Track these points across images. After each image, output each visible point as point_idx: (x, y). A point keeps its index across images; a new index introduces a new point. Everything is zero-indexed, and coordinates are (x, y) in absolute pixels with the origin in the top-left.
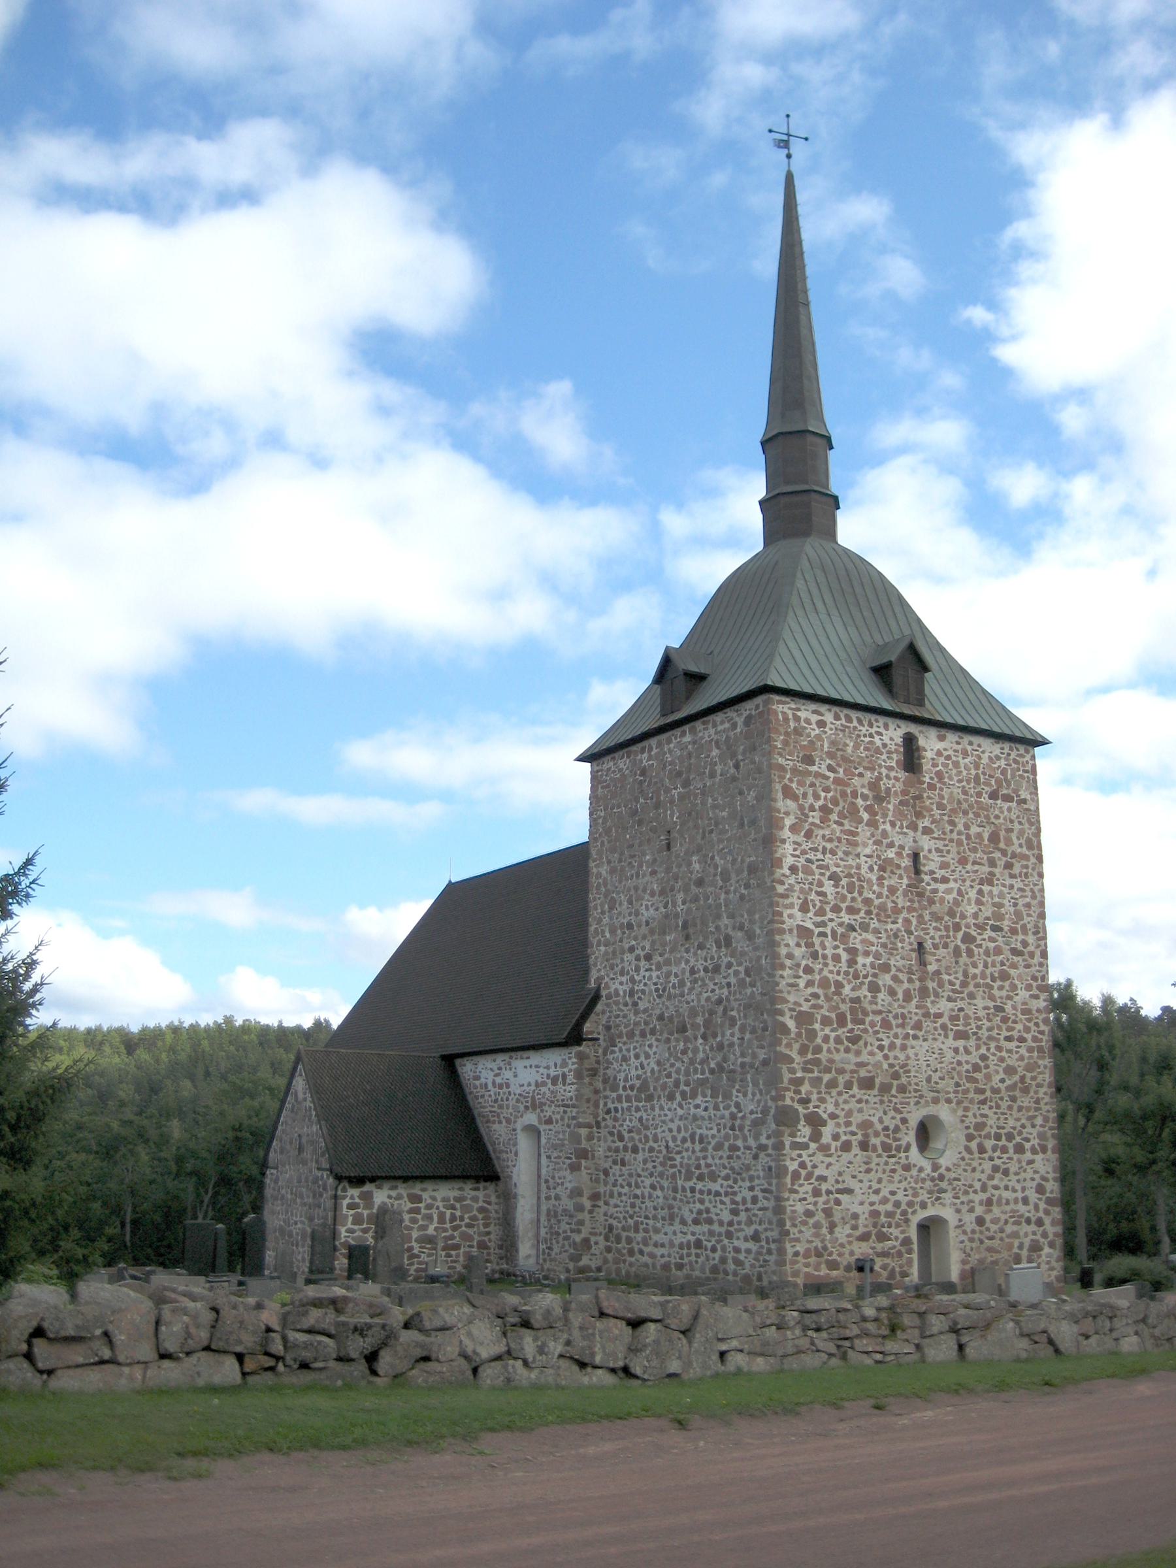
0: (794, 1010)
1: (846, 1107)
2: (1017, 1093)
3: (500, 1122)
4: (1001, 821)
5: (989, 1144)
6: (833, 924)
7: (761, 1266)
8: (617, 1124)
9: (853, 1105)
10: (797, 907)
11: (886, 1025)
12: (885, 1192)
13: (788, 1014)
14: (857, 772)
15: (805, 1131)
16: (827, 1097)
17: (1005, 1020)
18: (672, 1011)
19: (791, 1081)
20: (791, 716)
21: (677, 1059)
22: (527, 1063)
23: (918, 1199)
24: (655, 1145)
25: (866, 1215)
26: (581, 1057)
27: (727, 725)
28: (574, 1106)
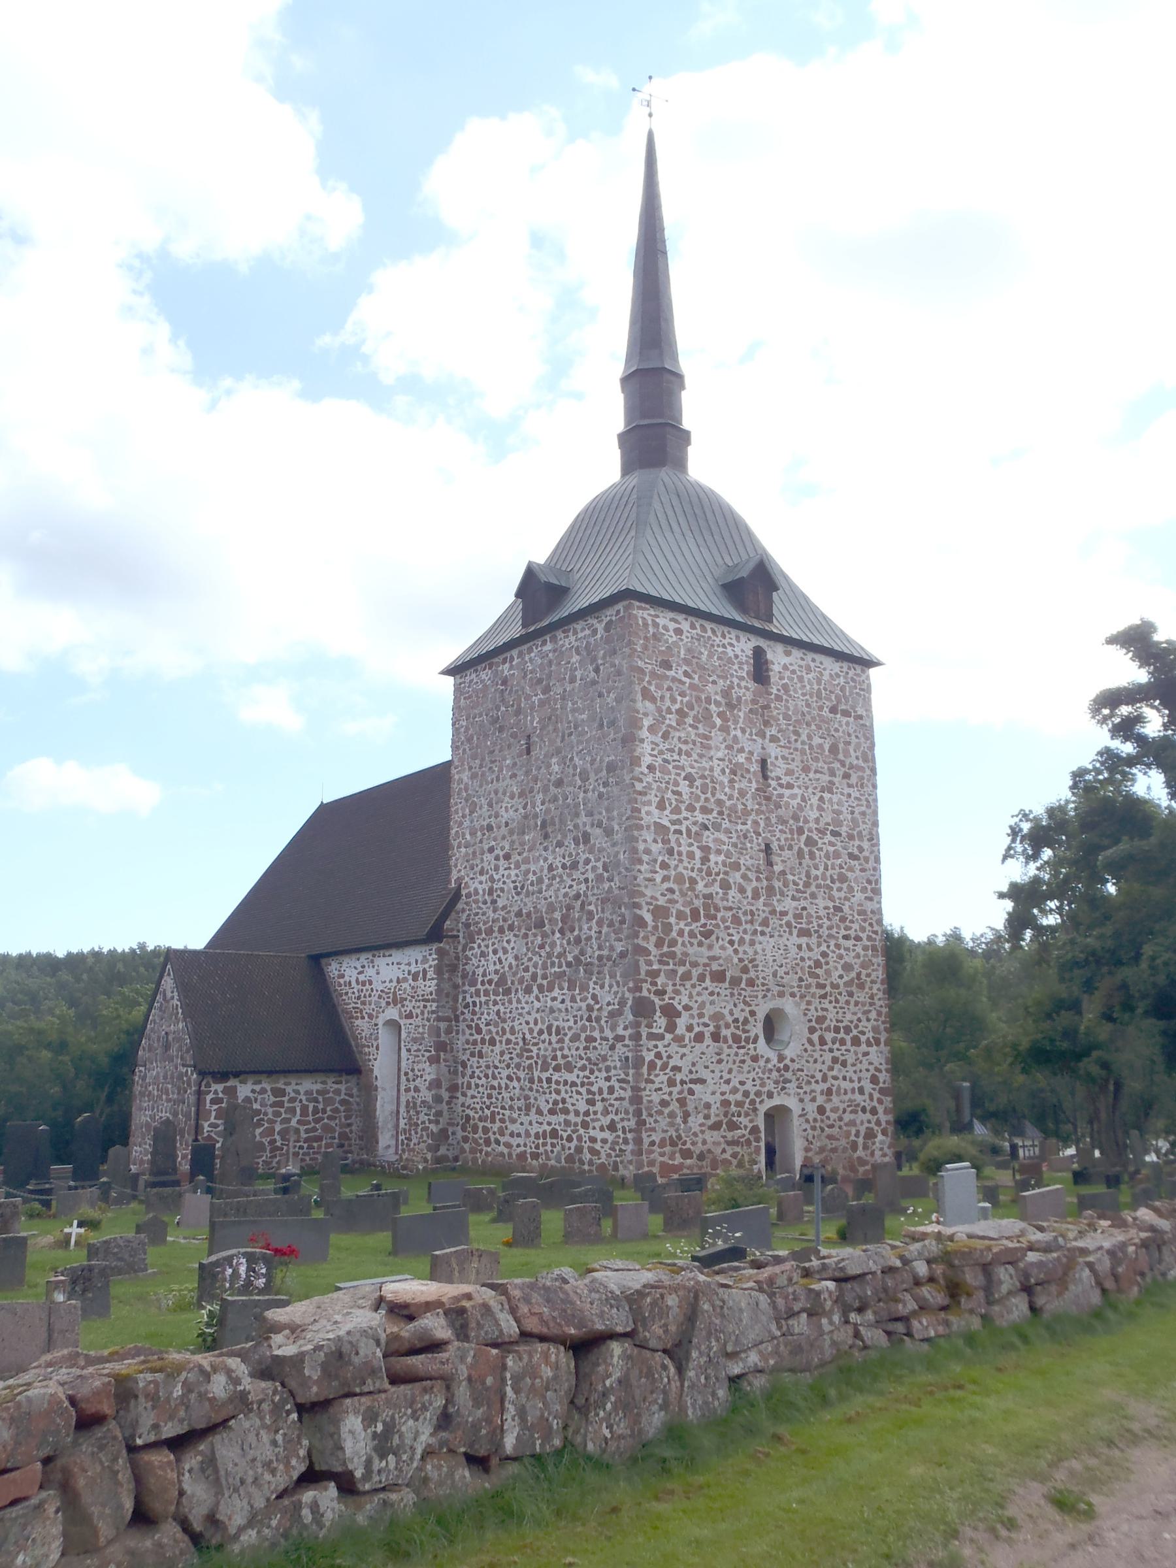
0: (651, 904)
1: (700, 999)
2: (854, 989)
3: (363, 1018)
4: (841, 734)
5: (829, 1036)
6: (688, 822)
7: (617, 1156)
8: (475, 1018)
9: (705, 997)
10: (654, 805)
11: (736, 920)
12: (735, 1083)
13: (645, 908)
14: (711, 679)
15: (661, 1022)
16: (682, 989)
17: (843, 919)
18: (530, 907)
19: (648, 973)
20: (650, 622)
21: (535, 953)
22: (389, 960)
23: (766, 1089)
24: (512, 1038)
25: (718, 1105)
26: (441, 953)
27: (587, 632)
28: (433, 1001)
